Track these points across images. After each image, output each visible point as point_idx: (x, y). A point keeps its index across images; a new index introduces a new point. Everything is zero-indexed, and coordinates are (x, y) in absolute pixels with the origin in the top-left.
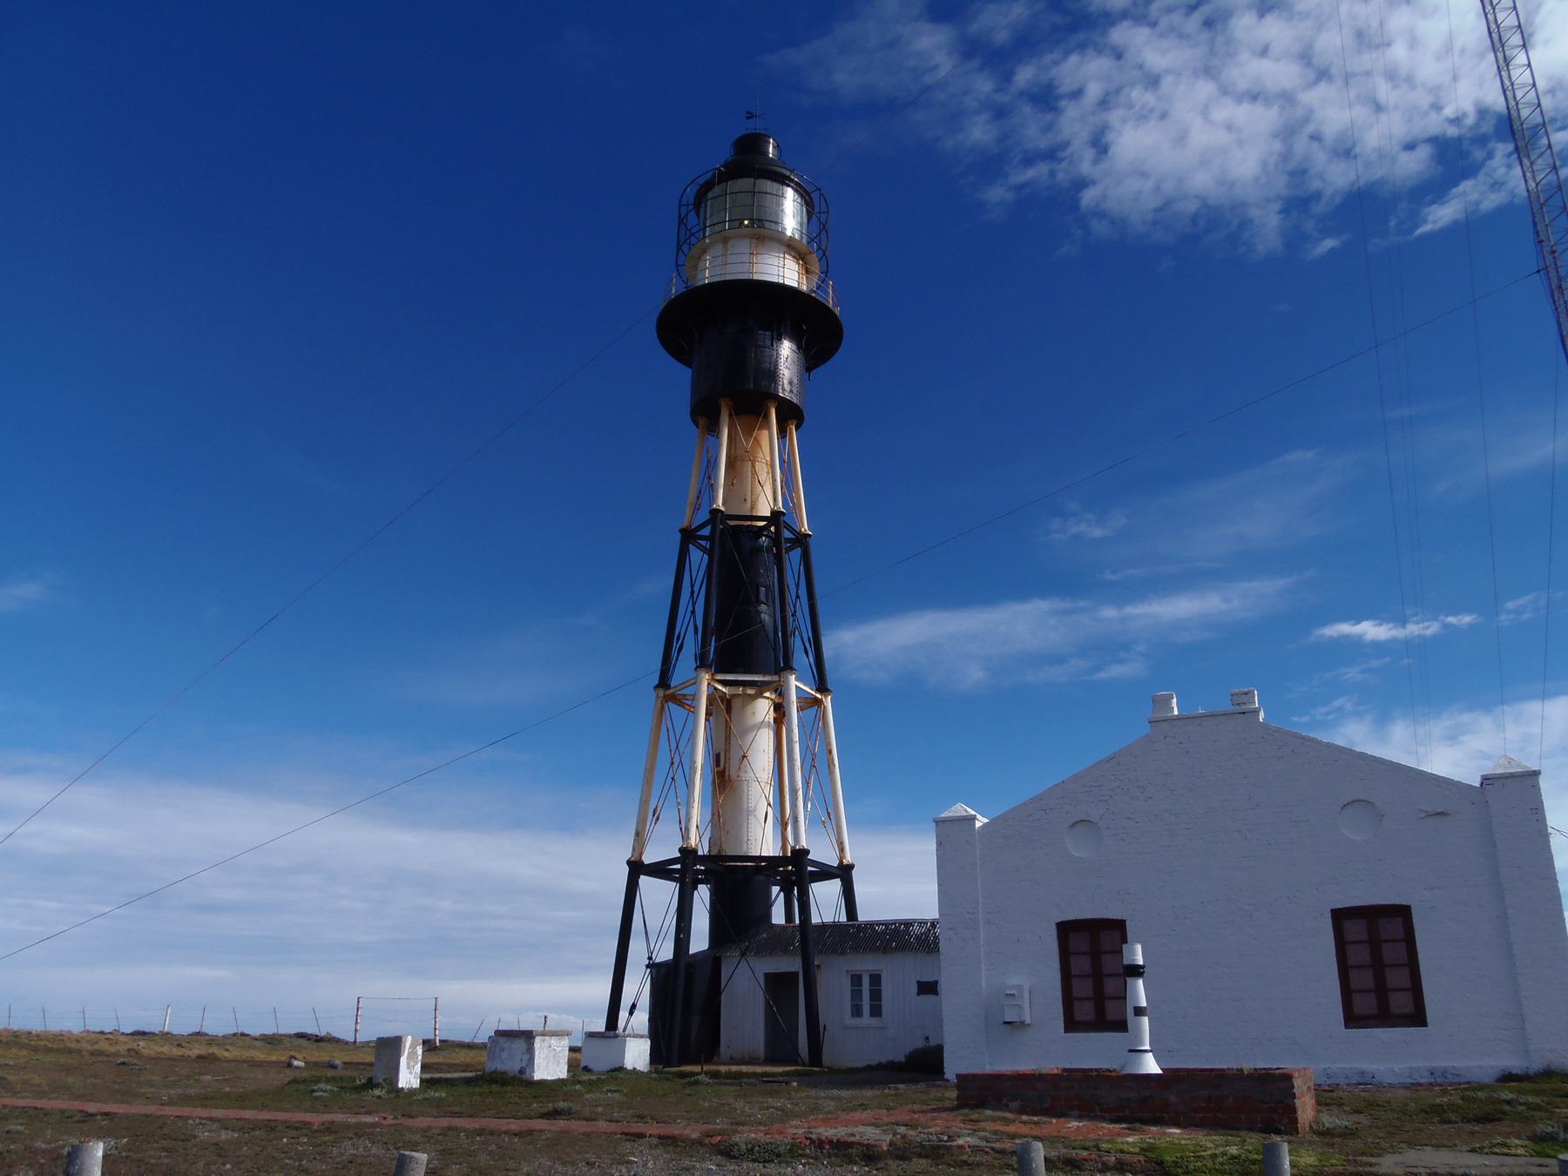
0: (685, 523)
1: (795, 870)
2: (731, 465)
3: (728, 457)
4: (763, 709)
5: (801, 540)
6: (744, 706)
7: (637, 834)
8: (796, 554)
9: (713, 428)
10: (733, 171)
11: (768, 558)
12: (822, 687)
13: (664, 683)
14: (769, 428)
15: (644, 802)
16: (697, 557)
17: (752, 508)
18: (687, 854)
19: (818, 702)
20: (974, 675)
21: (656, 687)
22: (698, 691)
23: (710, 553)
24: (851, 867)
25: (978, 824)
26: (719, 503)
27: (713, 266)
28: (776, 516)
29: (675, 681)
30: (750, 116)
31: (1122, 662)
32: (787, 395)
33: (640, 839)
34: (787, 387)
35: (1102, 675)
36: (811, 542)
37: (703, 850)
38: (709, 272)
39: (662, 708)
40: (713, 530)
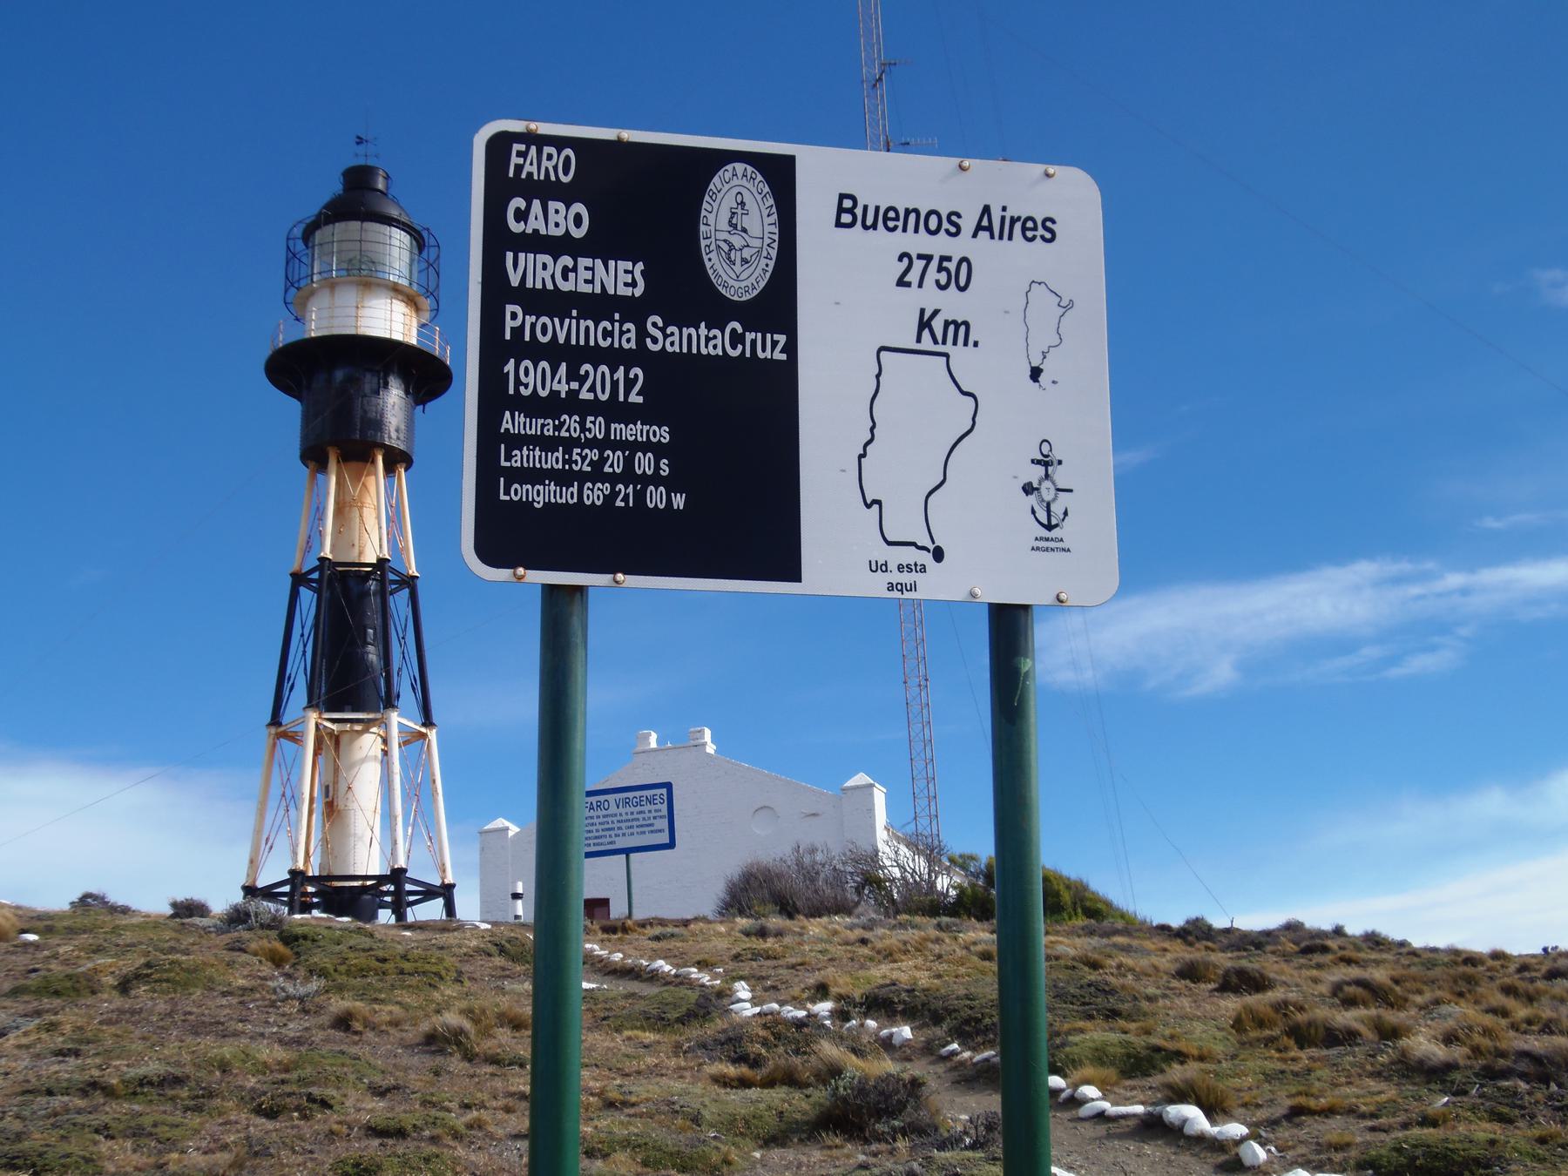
0: (295, 567)
1: (395, 887)
2: (339, 511)
3: (337, 502)
4: (369, 743)
5: (409, 582)
6: (352, 741)
7: (252, 861)
8: (405, 593)
9: (322, 467)
10: (338, 211)
11: (374, 602)
12: (428, 722)
13: (276, 720)
14: (376, 474)
15: (258, 831)
16: (307, 597)
17: (360, 553)
18: (297, 877)
19: (424, 736)
20: (1223, 673)
21: (269, 725)
22: (307, 728)
23: (318, 591)
24: (453, 886)
25: (511, 834)
26: (327, 552)
27: (319, 318)
28: (382, 562)
29: (287, 719)
30: (360, 141)
31: (1433, 649)
32: (394, 443)
33: (254, 864)
34: (394, 435)
35: (1395, 672)
36: (419, 583)
37: (313, 871)
38: (318, 323)
39: (274, 745)
40: (321, 575)
